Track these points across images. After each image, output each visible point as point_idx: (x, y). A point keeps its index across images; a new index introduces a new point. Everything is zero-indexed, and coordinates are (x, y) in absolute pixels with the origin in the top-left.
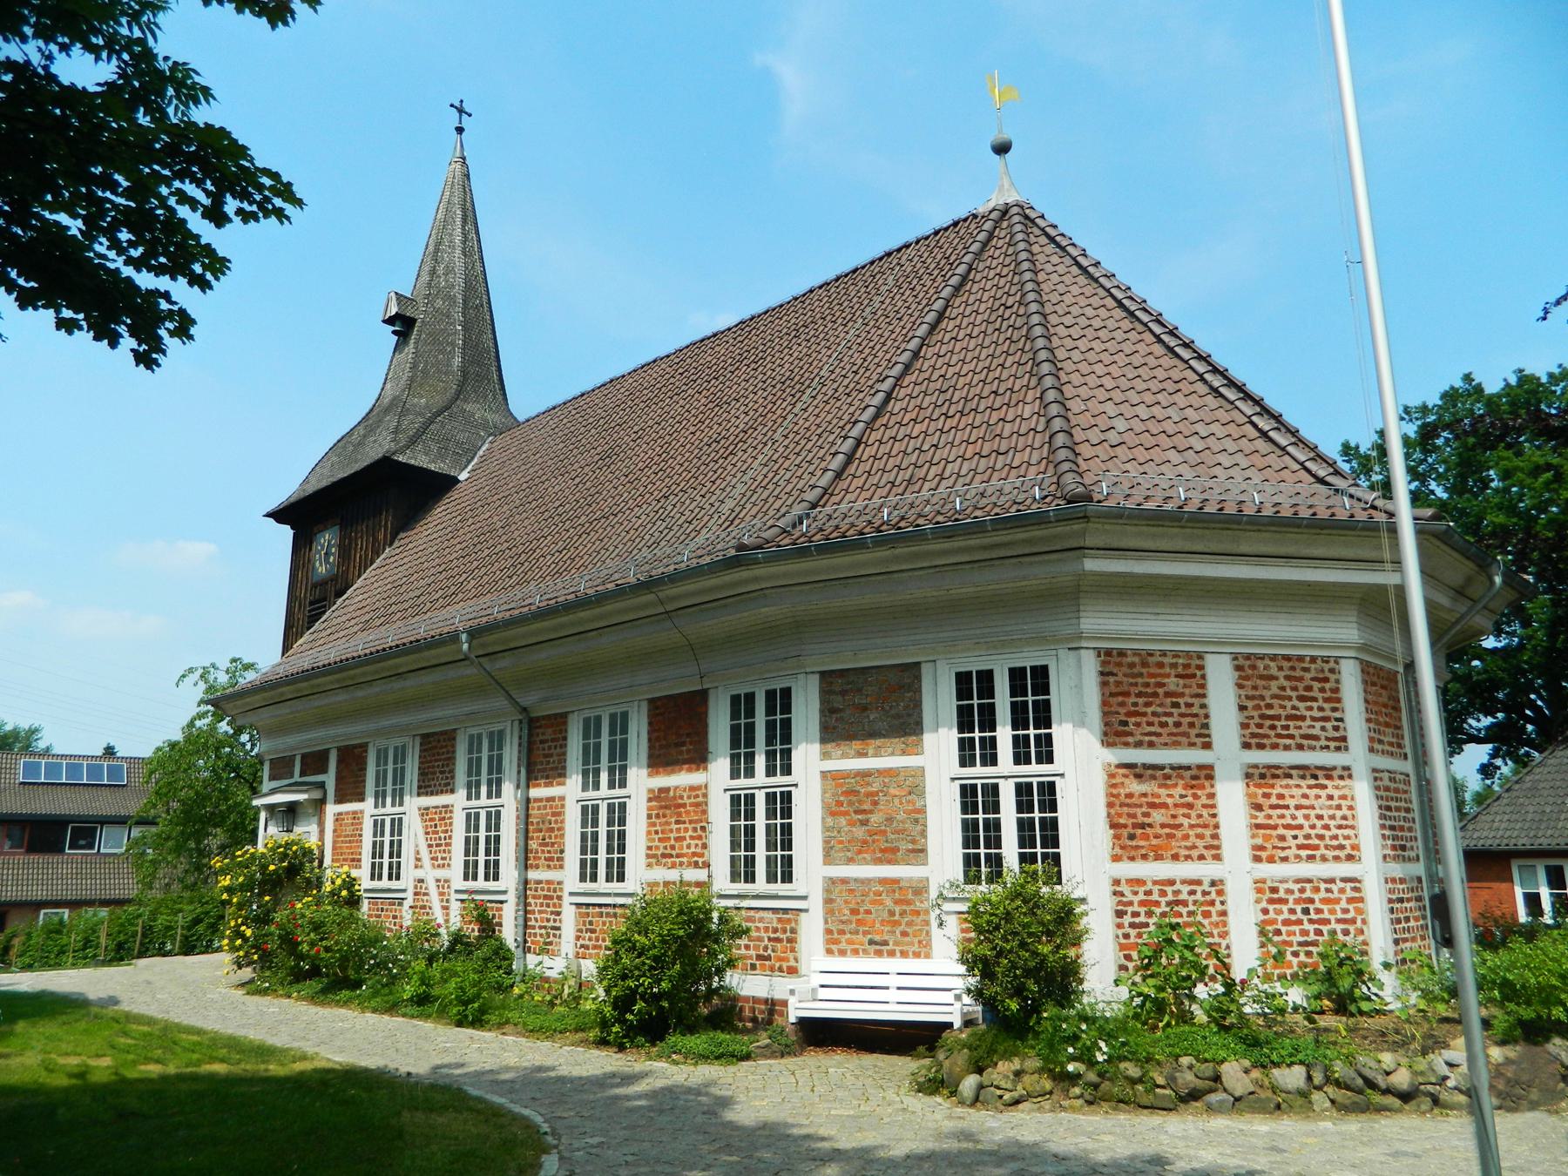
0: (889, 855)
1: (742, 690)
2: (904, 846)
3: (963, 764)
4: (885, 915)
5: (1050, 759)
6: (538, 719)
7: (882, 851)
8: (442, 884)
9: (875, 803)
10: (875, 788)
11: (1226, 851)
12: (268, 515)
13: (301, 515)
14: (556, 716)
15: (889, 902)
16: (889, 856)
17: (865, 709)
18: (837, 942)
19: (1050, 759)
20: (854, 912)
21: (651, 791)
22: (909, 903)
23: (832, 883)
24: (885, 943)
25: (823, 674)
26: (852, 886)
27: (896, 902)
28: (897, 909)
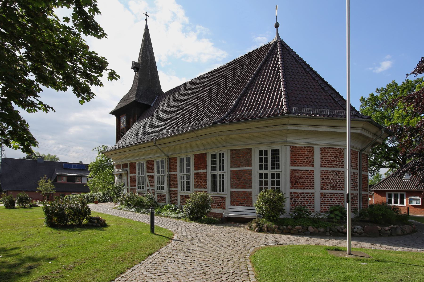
0: (244, 187)
2: (247, 185)
3: (260, 169)
5: (279, 169)
10: (242, 173)
19: (279, 169)
20: (237, 197)
21: (195, 173)
23: (232, 192)
25: (231, 150)
27: (245, 196)
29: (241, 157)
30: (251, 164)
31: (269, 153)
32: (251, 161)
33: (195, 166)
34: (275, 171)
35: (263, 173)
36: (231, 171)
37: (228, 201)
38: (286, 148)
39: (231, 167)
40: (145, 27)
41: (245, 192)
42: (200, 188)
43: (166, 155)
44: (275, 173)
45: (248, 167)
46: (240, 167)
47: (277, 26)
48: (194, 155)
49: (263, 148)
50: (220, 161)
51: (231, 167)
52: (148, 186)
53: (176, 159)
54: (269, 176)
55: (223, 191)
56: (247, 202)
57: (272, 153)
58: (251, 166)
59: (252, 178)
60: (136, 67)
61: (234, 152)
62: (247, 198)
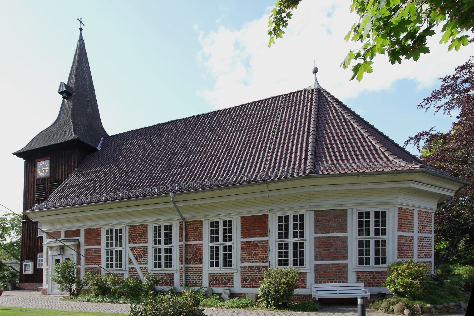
0: (336, 258)
1: (283, 214)
2: (340, 256)
3: (155, 244)
4: (334, 273)
5: (303, 237)
6: (188, 222)
7: (333, 257)
8: (144, 270)
9: (332, 245)
10: (332, 241)
11: (148, 262)
12: (14, 154)
13: (30, 156)
14: (200, 221)
15: (335, 270)
16: (336, 258)
17: (329, 221)
18: (318, 280)
19: (303, 237)
20: (324, 272)
21: (242, 242)
22: (341, 269)
23: (317, 266)
24: (334, 279)
25: (315, 211)
26: (324, 266)
27: (337, 270)
28: (338, 271)
29: (331, 220)
30: (347, 229)
31: (163, 229)
32: (346, 225)
33: (242, 233)
34: (283, 241)
35: (227, 245)
36: (315, 238)
37: (310, 278)
38: (395, 210)
39: (316, 233)
40: (78, 39)
41: (338, 264)
42: (253, 262)
43: (182, 217)
44: (283, 243)
45: (341, 232)
46: (329, 233)
47: (315, 71)
48: (242, 217)
49: (109, 228)
50: (116, 237)
51: (316, 233)
52: (130, 262)
53: (199, 224)
54: (221, 249)
55: (121, 267)
56: (339, 277)
57: (225, 225)
58: (346, 232)
59: (347, 247)
60: (66, 93)
61: (320, 214)
62: (339, 272)
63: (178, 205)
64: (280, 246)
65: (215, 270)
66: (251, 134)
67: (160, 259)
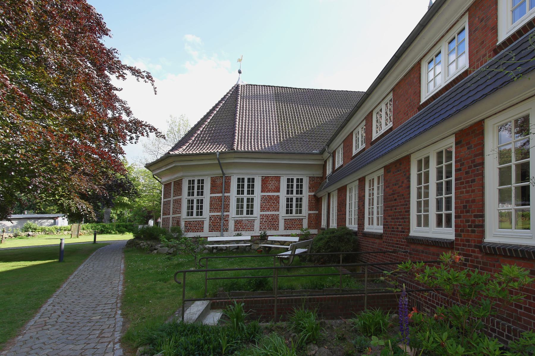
23: (309, 214)
34: (250, 196)
47: (240, 60)
57: (249, 181)
63: (221, 162)
64: (238, 200)
65: (289, 216)
66: (263, 106)
67: (192, 209)
